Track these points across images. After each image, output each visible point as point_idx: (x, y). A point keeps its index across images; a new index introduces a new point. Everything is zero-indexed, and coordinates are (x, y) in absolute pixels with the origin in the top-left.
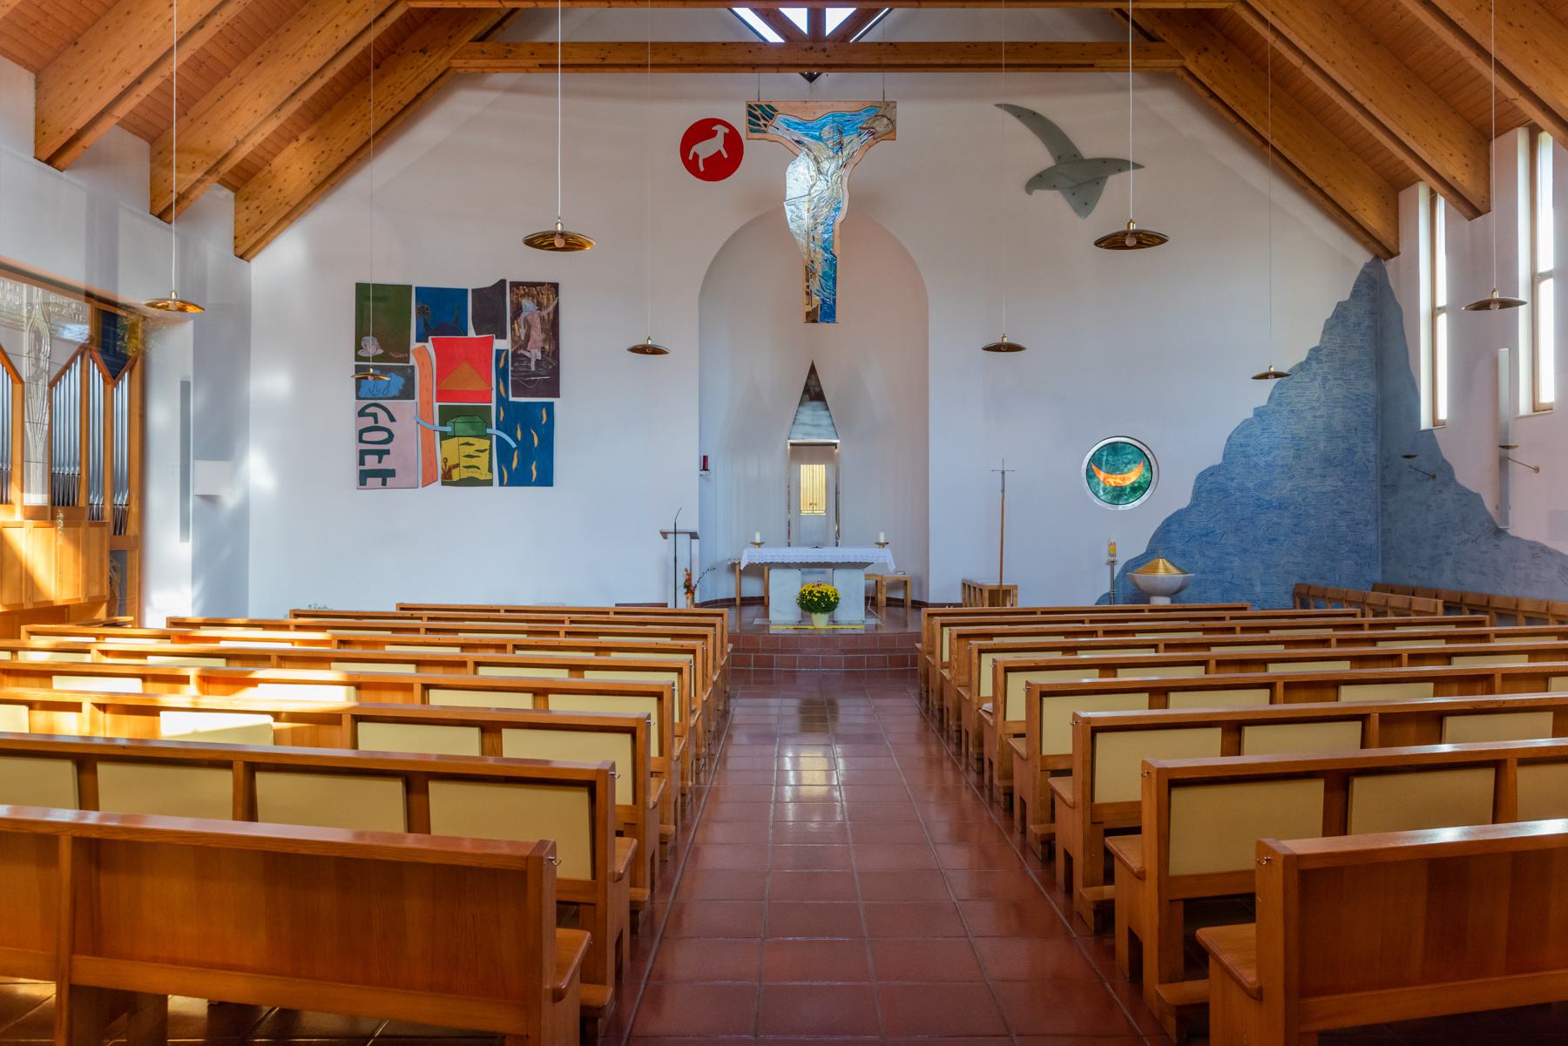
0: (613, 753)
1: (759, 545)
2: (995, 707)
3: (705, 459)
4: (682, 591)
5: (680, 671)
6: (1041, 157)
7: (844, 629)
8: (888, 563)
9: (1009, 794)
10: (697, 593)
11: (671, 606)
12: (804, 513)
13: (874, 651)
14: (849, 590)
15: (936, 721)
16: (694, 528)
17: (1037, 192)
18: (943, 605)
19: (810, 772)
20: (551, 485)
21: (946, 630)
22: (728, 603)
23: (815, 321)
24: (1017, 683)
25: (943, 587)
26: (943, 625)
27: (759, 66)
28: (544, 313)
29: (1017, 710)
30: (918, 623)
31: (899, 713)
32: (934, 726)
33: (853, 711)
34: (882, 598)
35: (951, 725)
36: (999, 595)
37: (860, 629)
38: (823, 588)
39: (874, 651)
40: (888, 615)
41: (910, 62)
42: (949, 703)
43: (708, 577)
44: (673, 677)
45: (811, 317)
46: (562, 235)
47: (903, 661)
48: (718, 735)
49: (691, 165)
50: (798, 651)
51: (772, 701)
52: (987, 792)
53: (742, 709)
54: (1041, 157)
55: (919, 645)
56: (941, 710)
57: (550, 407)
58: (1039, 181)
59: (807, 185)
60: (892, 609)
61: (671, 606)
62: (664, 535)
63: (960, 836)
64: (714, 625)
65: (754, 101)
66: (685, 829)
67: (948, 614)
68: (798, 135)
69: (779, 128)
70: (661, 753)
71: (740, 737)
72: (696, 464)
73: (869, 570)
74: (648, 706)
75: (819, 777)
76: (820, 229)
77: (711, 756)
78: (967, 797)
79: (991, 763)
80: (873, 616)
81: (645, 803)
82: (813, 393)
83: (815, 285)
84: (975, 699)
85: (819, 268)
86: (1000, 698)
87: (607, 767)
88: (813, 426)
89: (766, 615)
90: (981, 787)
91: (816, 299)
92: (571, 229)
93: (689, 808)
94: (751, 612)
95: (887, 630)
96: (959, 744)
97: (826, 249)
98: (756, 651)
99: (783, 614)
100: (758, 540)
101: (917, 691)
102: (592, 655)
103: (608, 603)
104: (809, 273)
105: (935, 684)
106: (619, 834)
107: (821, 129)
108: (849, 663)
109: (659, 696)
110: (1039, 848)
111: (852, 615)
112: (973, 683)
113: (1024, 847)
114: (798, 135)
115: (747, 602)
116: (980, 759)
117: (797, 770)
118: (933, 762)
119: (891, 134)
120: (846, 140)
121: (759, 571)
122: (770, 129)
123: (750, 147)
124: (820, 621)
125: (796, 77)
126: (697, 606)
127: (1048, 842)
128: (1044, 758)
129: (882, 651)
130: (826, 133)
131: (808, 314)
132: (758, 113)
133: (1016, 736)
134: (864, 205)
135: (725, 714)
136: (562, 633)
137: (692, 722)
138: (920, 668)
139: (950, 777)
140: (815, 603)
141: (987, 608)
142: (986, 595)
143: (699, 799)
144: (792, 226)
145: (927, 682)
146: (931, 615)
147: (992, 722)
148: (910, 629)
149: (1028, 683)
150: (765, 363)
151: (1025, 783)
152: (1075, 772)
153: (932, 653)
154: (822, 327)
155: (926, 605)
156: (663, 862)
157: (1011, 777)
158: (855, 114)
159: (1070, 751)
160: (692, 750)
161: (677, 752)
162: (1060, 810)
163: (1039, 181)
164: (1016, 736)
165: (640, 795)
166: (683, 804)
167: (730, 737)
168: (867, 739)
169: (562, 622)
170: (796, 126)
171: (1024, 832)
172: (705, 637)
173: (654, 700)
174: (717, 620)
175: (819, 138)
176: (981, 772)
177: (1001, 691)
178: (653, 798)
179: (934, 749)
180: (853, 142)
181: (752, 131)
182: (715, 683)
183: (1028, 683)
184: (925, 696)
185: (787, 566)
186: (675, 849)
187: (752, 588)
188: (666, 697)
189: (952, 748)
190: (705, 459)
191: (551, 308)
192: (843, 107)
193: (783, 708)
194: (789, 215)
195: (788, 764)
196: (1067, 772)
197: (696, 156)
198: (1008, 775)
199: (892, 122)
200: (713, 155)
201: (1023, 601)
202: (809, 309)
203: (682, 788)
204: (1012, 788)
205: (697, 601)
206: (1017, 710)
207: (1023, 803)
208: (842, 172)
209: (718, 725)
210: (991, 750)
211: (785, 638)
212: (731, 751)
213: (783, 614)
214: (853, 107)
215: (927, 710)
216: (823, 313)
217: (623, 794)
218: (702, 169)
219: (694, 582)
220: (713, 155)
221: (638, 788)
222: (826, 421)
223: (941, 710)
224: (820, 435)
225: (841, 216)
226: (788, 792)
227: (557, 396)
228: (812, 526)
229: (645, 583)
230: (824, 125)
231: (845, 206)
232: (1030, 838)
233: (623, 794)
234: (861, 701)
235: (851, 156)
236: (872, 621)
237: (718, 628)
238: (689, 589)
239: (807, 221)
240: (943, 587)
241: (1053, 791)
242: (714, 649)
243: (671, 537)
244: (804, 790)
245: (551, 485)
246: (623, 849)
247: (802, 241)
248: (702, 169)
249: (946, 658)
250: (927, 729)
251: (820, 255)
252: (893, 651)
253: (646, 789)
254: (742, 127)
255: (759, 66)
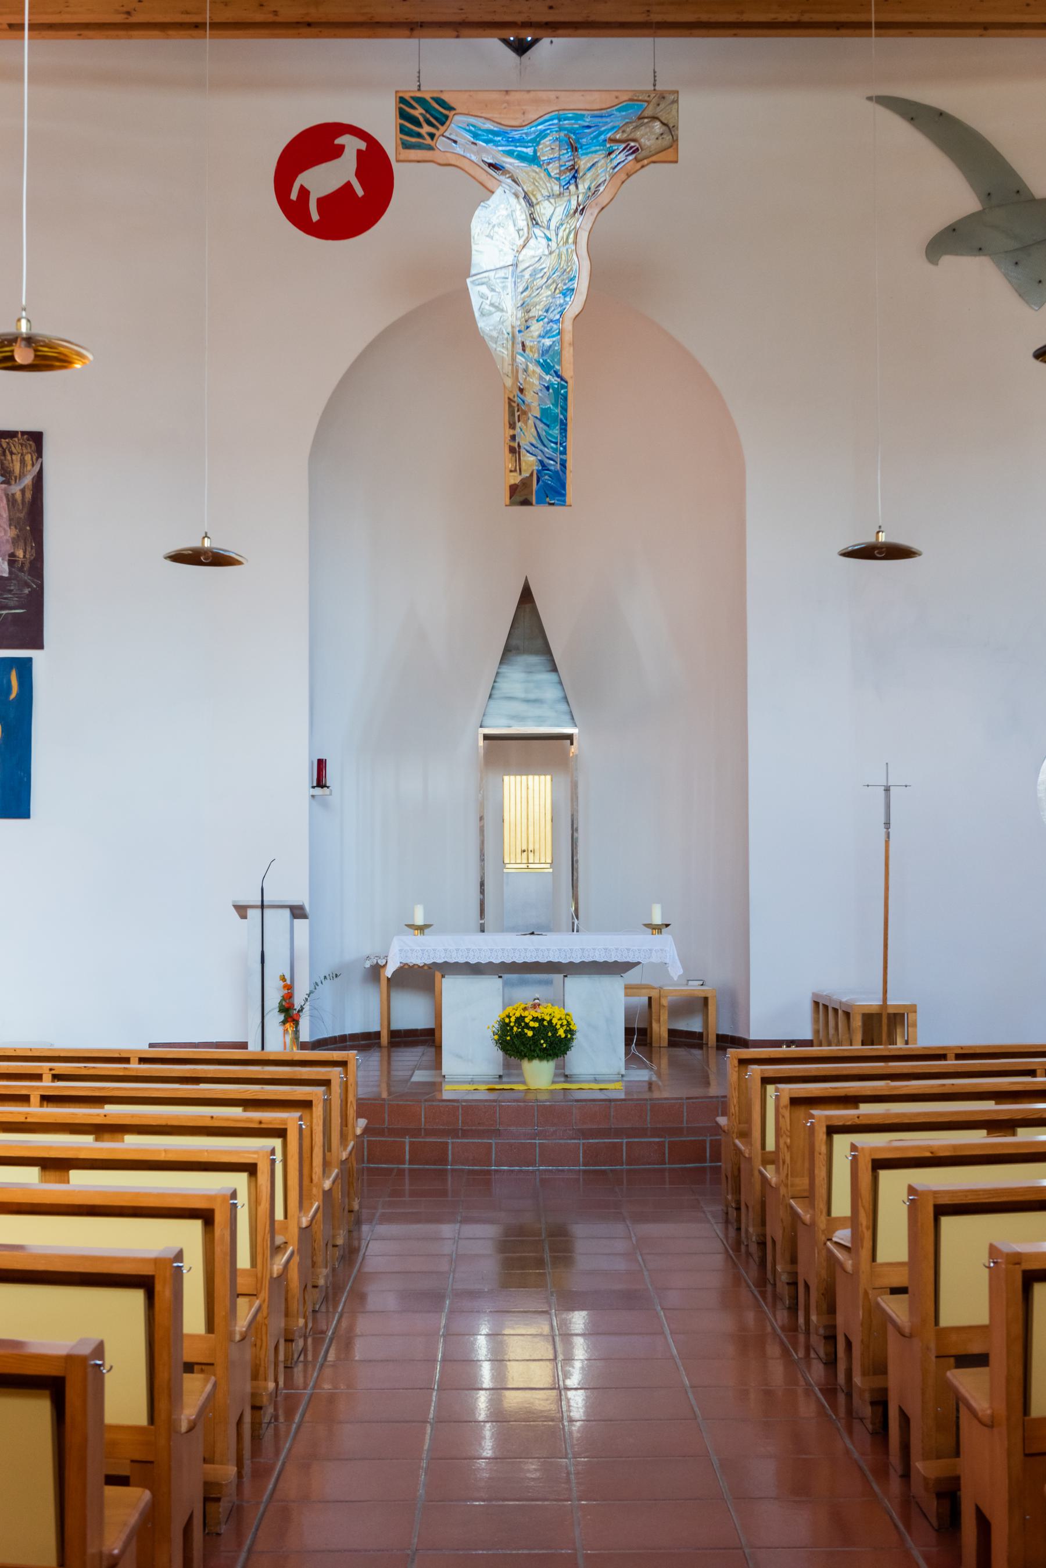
0: (114, 1324)
1: (422, 929)
2: (856, 1236)
3: (321, 764)
4: (274, 1019)
5: (251, 1169)
6: (955, 196)
7: (588, 1090)
8: (669, 963)
9: (880, 1402)
10: (304, 1023)
11: (254, 1047)
12: (510, 868)
13: (642, 1132)
14: (596, 1017)
15: (754, 1267)
16: (300, 897)
17: (948, 261)
18: (777, 1044)
19: (532, 1368)
20: (25, 814)
21: (771, 1089)
22: (366, 1041)
23: (526, 502)
24: (894, 1185)
25: (777, 1011)
26: (766, 1081)
27: (422, 25)
28: (16, 489)
29: (893, 1244)
30: (727, 1075)
31: (689, 1249)
32: (750, 1275)
33: (601, 1247)
34: (660, 1030)
35: (781, 1272)
36: (883, 1023)
37: (616, 1090)
38: (544, 1012)
39: (642, 1132)
40: (673, 1063)
41: (705, 17)
42: (775, 1230)
43: (327, 989)
44: (239, 1181)
45: (520, 495)
46: (29, 340)
47: (697, 1152)
48: (331, 1294)
49: (295, 210)
50: (497, 1133)
51: (447, 1230)
52: (842, 1398)
53: (384, 1245)
54: (955, 196)
55: (722, 1121)
56: (762, 1244)
57: (25, 667)
58: (953, 239)
59: (513, 248)
60: (681, 1053)
61: (254, 1047)
62: (242, 910)
63: (798, 1487)
64: (326, 1083)
65: (409, 89)
66: (261, 1473)
67: (781, 1060)
68: (494, 153)
69: (457, 139)
70: (210, 1327)
71: (382, 1297)
72: (306, 775)
73: (632, 977)
74: (188, 1235)
75: (541, 1374)
76: (536, 328)
77: (318, 1336)
78: (807, 1409)
79: (849, 1344)
80: (642, 1065)
81: (172, 1425)
82: (527, 632)
83: (527, 435)
84: (822, 1222)
85: (535, 401)
86: (864, 1220)
87: (86, 1350)
88: (526, 703)
89: (438, 1064)
90: (830, 1391)
91: (530, 462)
92: (44, 330)
93: (268, 1434)
94: (408, 1058)
95: (670, 1091)
96: (793, 1309)
97: (546, 367)
98: (416, 1132)
99: (469, 1059)
100: (419, 921)
101: (719, 1208)
102: (89, 1139)
103: (136, 1042)
104: (515, 412)
105: (750, 1195)
106: (113, 1480)
107: (536, 141)
108: (593, 1155)
109: (206, 1217)
110: (931, 1505)
111: (600, 1060)
112: (817, 1193)
113: (907, 1502)
114: (494, 153)
115: (403, 1039)
116: (831, 1338)
117: (499, 1361)
118: (749, 1344)
119: (669, 148)
120: (583, 163)
121: (421, 979)
122: (441, 143)
123: (406, 174)
124: (539, 1074)
125: (493, 47)
126: (304, 1046)
127: (949, 1493)
128: (943, 1333)
129: (656, 1132)
130: (547, 149)
131: (513, 489)
132: (418, 112)
133: (895, 1291)
134: (618, 282)
135: (350, 1253)
136: (35, 1099)
137: (277, 1267)
138: (725, 1165)
139: (777, 1370)
140: (530, 1040)
141: (857, 1048)
142: (857, 1023)
143: (290, 1414)
144: (482, 323)
145: (737, 1190)
146: (744, 1062)
147: (849, 1264)
148: (714, 1091)
149: (911, 1190)
150: (436, 587)
151: (906, 1383)
152: (993, 1359)
153: (745, 1135)
154: (539, 513)
155: (744, 1043)
156: (211, 1535)
157: (885, 1372)
158: (601, 114)
159: (985, 1321)
160: (278, 1323)
161: (242, 1323)
162: (969, 1431)
163: (953, 239)
164: (895, 1291)
165: (162, 1405)
166: (256, 1426)
167: (360, 1297)
168: (620, 1304)
169: (38, 1077)
170: (490, 137)
171: (906, 1475)
172: (306, 1105)
173: (197, 1225)
174: (334, 1074)
175: (534, 160)
176: (831, 1363)
177: (866, 1202)
178: (189, 1412)
179: (750, 1317)
180: (598, 167)
181: (406, 146)
182: (327, 1194)
183: (911, 1190)
184: (733, 1219)
185: (476, 969)
186: (237, 1512)
187: (411, 1012)
188: (219, 1218)
189: (782, 1316)
190: (321, 764)
191: (28, 480)
192: (577, 102)
193: (471, 1242)
194: (475, 302)
195: (482, 1345)
196: (980, 1360)
197: (304, 193)
198: (879, 1368)
199: (670, 129)
200: (337, 192)
201: (926, 1036)
202: (515, 479)
203: (254, 1395)
204: (884, 1391)
205: (305, 1036)
206: (893, 1244)
207: (905, 1419)
208: (578, 221)
209: (327, 1278)
210: (850, 1320)
211: (469, 1109)
212: (363, 1325)
213: (469, 1059)
214: (597, 101)
215: (738, 1243)
216: (542, 488)
217: (124, 1400)
218: (315, 217)
219: (298, 1001)
220: (337, 192)
221: (159, 1391)
222: (552, 693)
223: (762, 1244)
224: (540, 720)
225: (575, 305)
226: (482, 1402)
227: (39, 645)
228: (523, 894)
229: (204, 1002)
230: (542, 135)
231: (582, 285)
232: (917, 1488)
233: (124, 1400)
234: (619, 1229)
235: (593, 192)
236: (642, 1075)
237: (336, 1088)
238: (289, 1013)
239: (512, 315)
240: (777, 1011)
241: (959, 1400)
242: (324, 1129)
243: (254, 914)
244: (513, 1400)
245: (25, 814)
246: (122, 1510)
247: (502, 351)
248: (315, 217)
249: (770, 1145)
250: (737, 1280)
251: (536, 379)
252: (679, 1131)
253: (175, 1396)
254: (388, 139)
255: (422, 25)
